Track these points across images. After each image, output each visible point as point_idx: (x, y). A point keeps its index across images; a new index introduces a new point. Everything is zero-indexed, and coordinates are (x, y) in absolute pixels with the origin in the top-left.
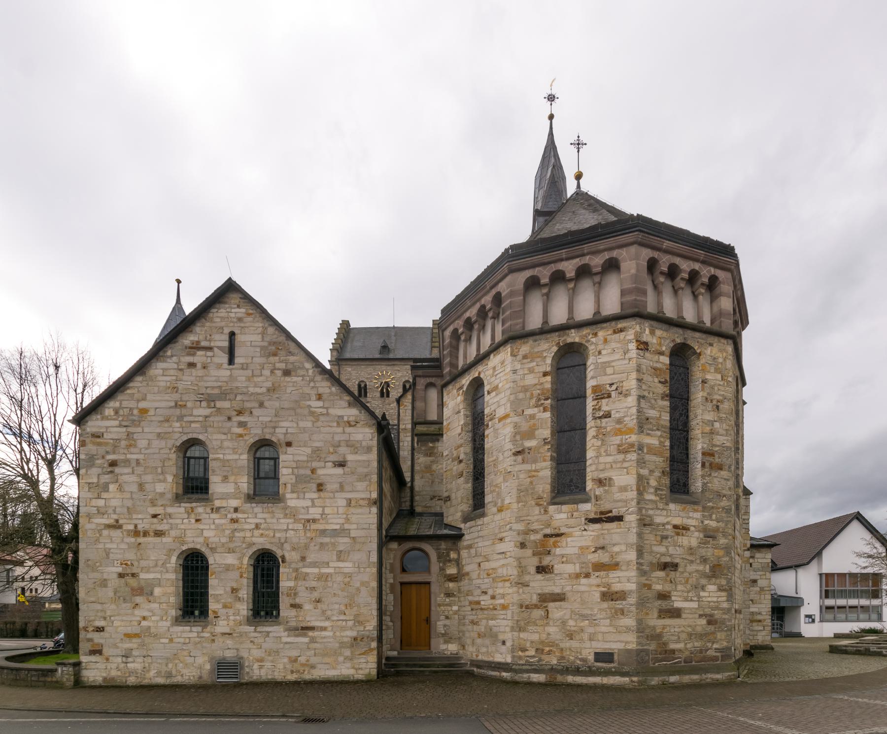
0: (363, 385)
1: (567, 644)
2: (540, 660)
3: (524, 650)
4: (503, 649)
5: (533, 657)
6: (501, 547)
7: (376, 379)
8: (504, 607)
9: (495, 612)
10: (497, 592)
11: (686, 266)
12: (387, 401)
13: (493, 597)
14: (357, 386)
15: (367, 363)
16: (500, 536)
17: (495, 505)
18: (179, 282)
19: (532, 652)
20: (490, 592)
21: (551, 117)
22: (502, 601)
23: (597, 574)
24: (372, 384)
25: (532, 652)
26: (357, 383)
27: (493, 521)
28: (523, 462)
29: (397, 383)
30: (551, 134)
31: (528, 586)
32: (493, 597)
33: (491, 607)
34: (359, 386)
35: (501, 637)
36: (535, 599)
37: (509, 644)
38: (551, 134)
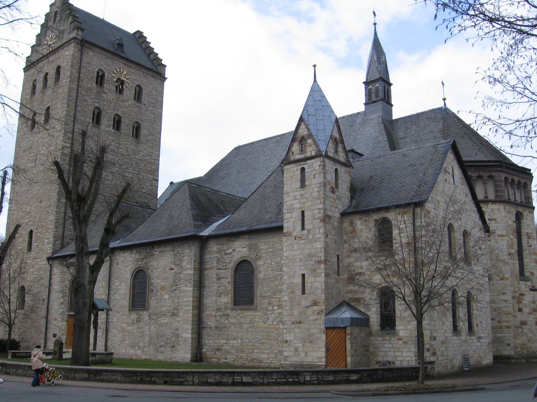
0: (101, 74)
1: (529, 345)
2: (522, 352)
3: (517, 348)
4: (508, 348)
5: (520, 351)
6: (504, 297)
7: (114, 73)
8: (508, 327)
9: (501, 330)
10: (503, 319)
11: (516, 179)
12: (121, 98)
13: (499, 322)
14: (96, 73)
15: (109, 55)
16: (504, 292)
17: (498, 276)
18: (315, 66)
19: (519, 349)
20: (497, 319)
21: (375, 24)
22: (506, 324)
23: (535, 313)
24: (109, 76)
25: (519, 349)
26: (97, 70)
27: (497, 284)
28: (511, 259)
29: (131, 85)
30: (376, 33)
31: (516, 317)
32: (499, 322)
33: (498, 327)
34: (98, 73)
35: (507, 342)
36: (519, 324)
37: (512, 345)
38: (376, 33)
